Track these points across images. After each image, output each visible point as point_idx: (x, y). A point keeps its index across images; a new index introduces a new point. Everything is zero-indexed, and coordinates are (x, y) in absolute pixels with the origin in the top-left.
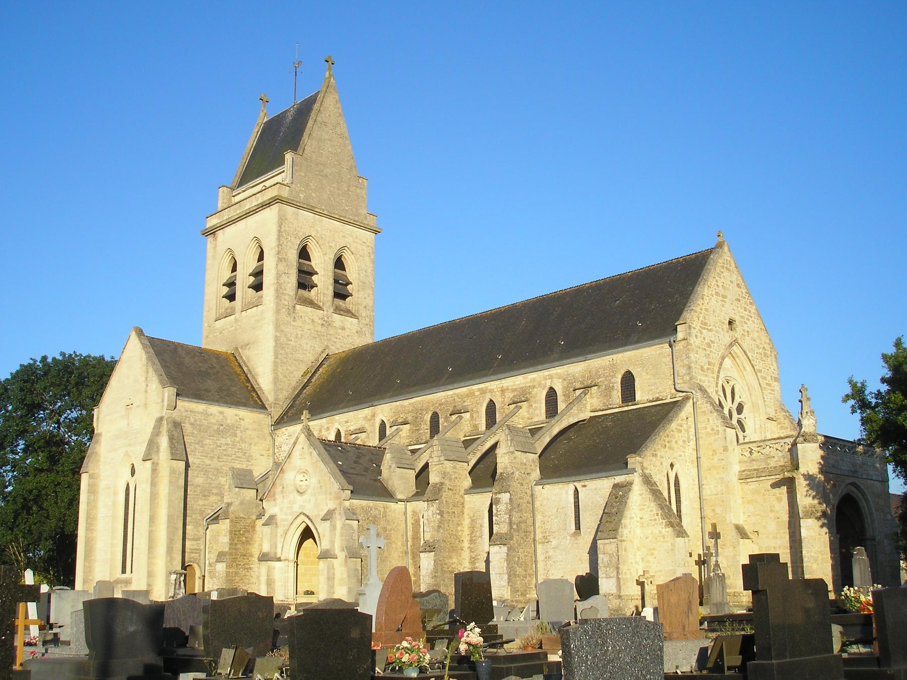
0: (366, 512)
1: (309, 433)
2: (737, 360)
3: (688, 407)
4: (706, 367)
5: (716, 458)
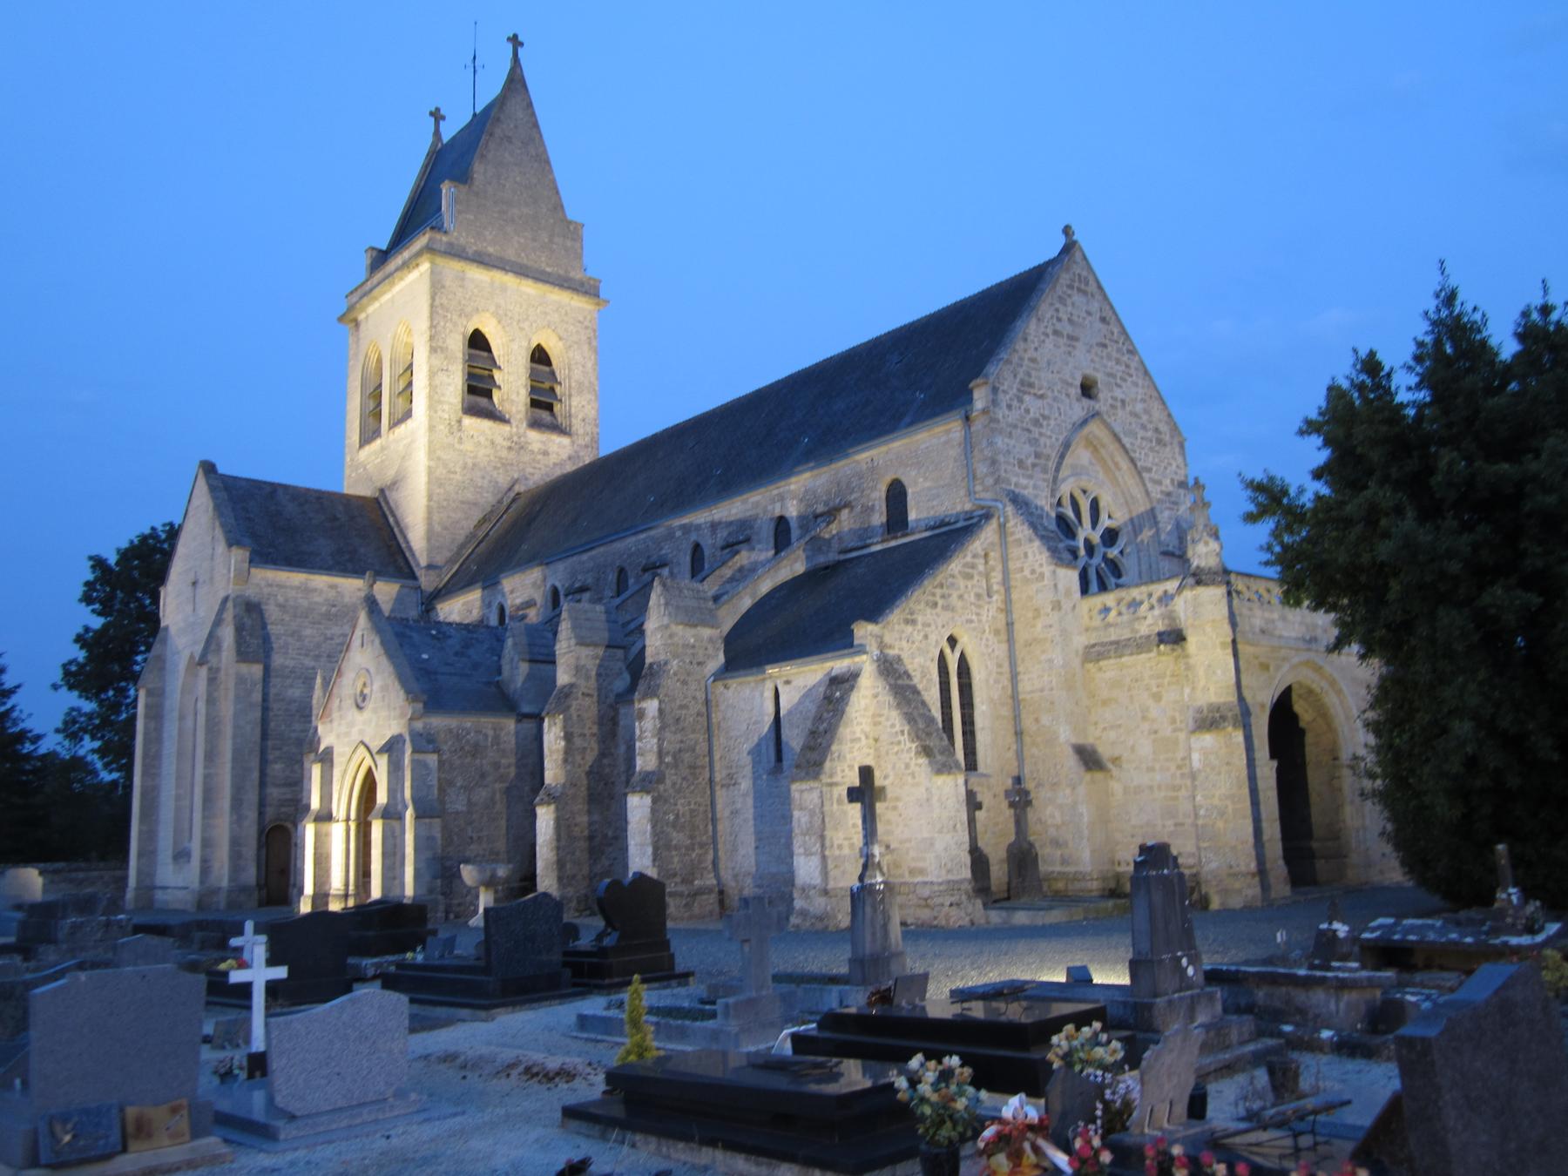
0: (458, 737)
2: (1102, 451)
3: (988, 534)
4: (1029, 461)
5: (1039, 625)
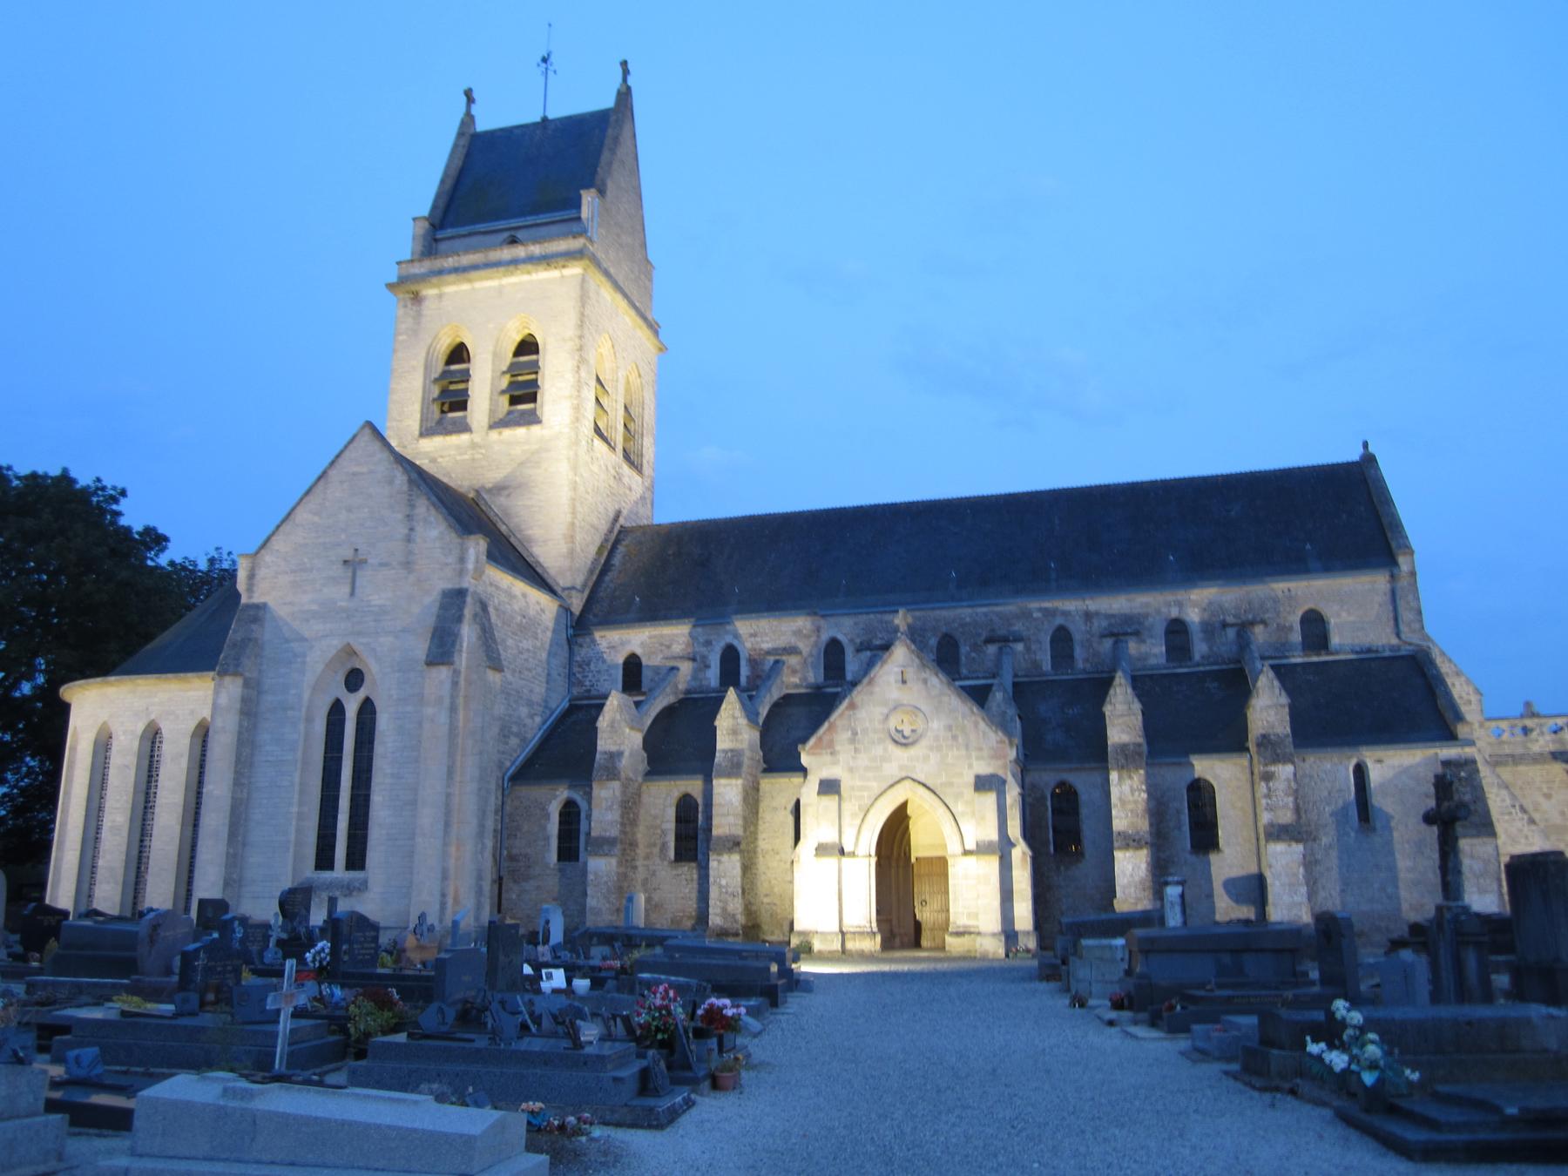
1: (792, 650)
